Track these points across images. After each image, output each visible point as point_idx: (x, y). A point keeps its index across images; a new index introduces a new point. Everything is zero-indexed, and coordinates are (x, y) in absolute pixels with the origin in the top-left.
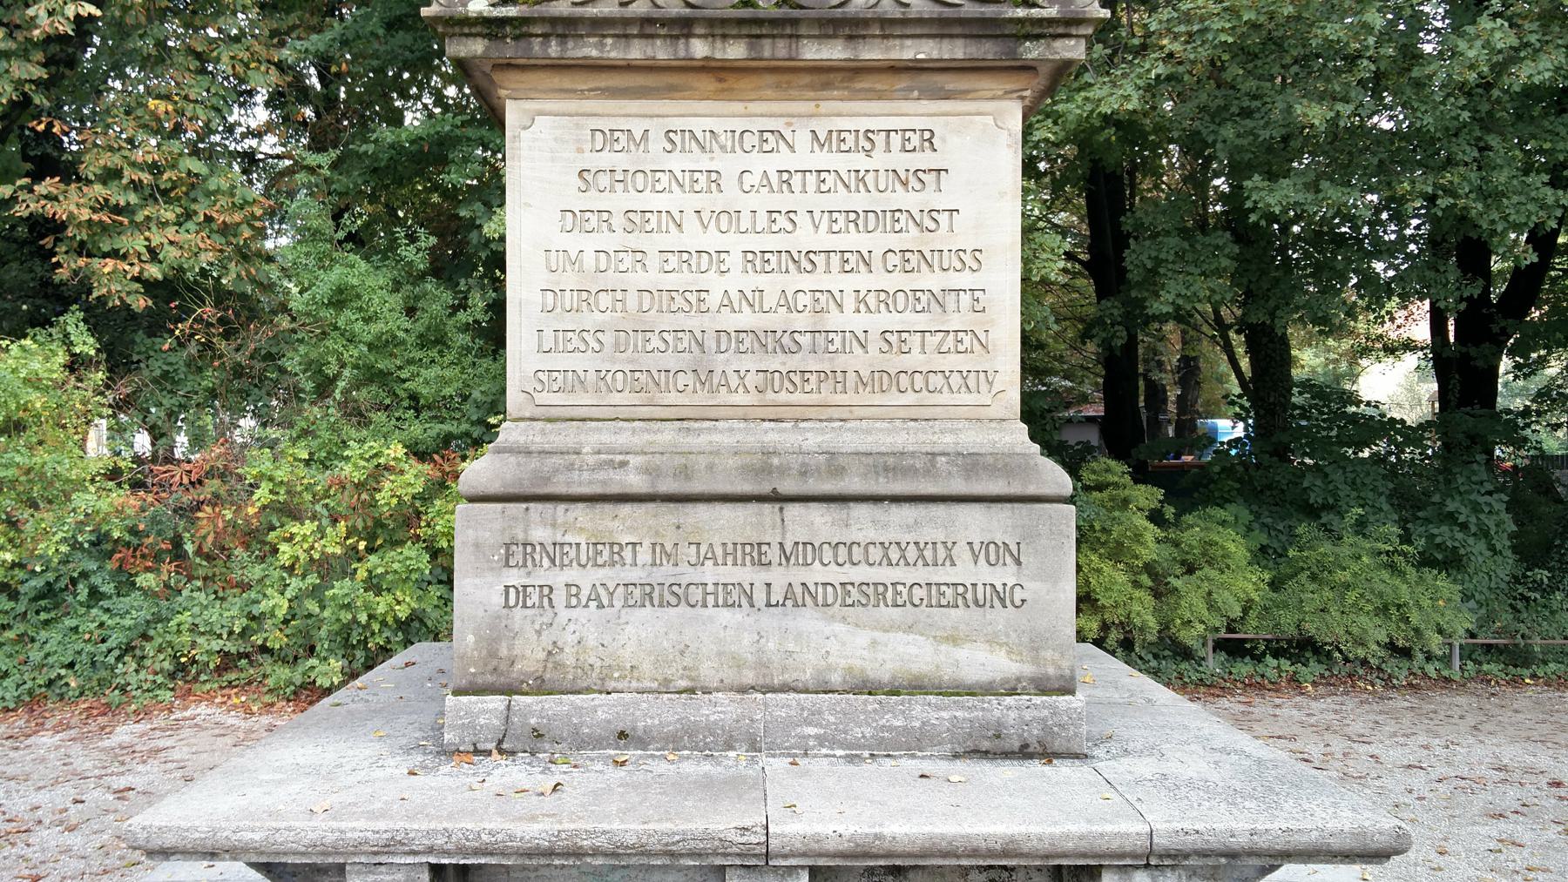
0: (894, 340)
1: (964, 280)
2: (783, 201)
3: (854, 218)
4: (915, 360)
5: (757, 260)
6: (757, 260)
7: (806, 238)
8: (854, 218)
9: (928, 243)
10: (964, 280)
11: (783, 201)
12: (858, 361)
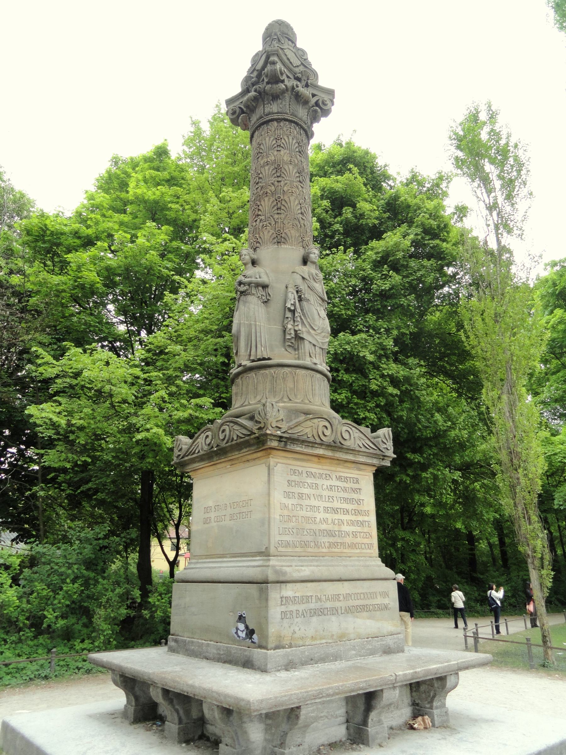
0: (355, 534)
2: (331, 494)
5: (326, 510)
6: (326, 510)
7: (336, 504)
9: (361, 508)
11: (331, 494)
12: (348, 540)
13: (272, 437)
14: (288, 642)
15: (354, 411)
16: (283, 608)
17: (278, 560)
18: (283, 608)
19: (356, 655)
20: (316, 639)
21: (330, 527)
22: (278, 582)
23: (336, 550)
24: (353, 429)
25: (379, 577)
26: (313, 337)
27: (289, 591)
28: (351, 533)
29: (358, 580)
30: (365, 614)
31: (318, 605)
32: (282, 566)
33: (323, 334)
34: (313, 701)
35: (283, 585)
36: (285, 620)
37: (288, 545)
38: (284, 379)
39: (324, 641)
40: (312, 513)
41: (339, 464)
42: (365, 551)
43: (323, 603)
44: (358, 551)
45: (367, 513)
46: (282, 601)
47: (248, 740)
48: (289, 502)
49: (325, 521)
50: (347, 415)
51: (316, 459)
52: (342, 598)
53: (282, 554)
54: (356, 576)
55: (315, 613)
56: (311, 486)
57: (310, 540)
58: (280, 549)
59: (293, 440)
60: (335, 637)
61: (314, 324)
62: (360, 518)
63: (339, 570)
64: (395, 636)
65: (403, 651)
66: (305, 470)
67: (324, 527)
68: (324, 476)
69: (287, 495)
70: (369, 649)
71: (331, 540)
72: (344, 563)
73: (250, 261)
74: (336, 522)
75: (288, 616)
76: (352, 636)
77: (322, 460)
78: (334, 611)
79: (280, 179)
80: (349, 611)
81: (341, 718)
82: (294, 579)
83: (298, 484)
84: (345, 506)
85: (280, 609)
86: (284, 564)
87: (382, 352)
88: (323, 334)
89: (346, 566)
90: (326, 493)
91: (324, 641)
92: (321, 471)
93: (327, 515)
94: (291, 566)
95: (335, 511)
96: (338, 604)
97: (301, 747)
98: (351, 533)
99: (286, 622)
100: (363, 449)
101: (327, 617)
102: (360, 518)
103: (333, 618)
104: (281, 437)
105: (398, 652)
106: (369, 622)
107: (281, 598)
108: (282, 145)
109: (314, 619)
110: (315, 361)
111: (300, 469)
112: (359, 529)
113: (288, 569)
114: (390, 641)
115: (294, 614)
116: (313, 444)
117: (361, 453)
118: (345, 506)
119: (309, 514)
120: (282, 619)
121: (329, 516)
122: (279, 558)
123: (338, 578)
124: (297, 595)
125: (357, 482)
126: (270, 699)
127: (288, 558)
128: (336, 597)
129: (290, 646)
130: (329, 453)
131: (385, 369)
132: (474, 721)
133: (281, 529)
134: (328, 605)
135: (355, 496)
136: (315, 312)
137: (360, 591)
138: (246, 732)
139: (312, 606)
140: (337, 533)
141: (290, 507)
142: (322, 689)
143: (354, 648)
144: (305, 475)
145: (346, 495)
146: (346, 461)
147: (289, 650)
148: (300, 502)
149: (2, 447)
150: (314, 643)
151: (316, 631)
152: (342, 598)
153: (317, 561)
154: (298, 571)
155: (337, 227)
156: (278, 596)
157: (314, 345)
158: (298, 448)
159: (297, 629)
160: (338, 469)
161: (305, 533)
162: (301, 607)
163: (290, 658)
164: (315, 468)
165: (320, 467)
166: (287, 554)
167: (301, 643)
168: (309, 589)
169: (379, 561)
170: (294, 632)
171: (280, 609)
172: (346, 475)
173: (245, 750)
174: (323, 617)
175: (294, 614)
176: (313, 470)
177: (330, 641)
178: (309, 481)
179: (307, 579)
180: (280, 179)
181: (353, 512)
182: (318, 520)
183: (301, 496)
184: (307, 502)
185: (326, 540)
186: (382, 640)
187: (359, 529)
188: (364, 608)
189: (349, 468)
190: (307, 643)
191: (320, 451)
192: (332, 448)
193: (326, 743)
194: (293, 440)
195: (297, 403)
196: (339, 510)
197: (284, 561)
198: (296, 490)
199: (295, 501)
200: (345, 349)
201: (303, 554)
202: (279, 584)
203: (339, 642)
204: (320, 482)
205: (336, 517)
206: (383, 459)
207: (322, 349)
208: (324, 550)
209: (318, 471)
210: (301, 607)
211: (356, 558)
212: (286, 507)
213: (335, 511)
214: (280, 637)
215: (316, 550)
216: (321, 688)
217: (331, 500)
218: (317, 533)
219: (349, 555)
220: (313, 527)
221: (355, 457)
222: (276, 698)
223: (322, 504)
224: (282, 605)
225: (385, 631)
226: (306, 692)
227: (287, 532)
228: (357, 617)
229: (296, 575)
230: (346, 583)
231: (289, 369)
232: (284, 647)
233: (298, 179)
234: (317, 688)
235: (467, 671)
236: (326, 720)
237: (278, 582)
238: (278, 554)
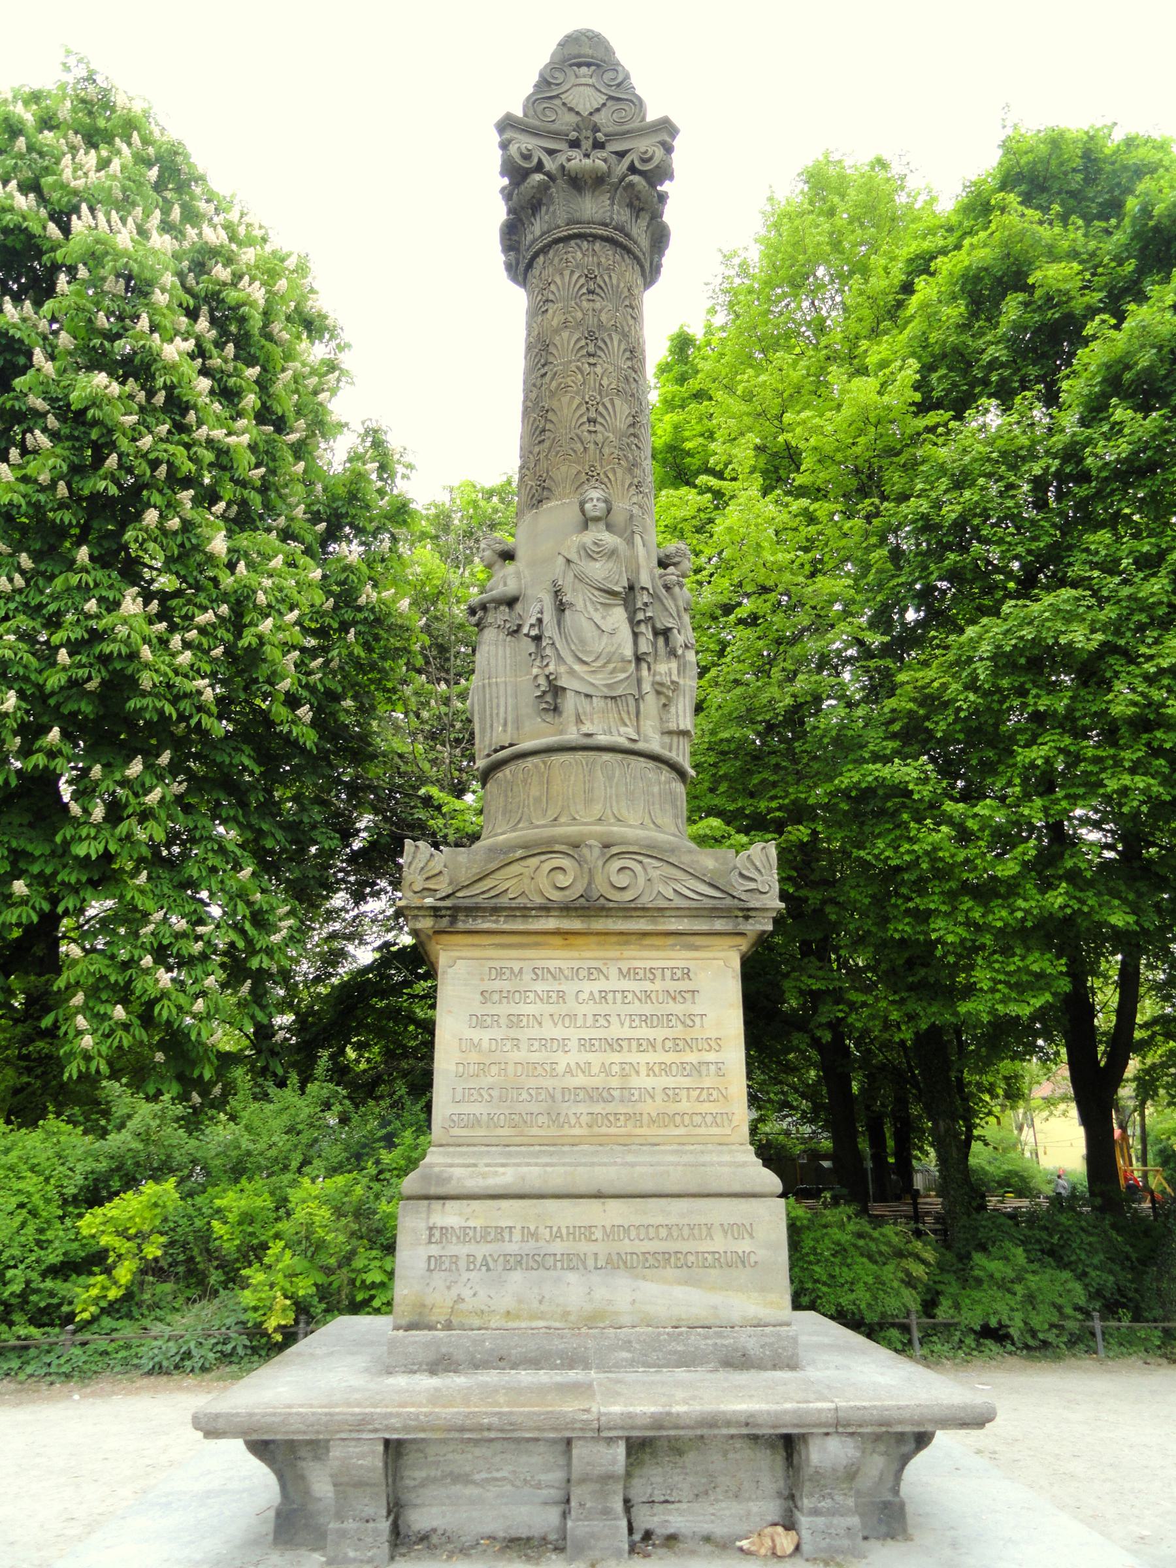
0: (671, 1094)
1: (711, 1057)
2: (603, 1009)
3: (645, 1019)
4: (684, 1106)
5: (586, 1045)
6: (586, 1045)
7: (616, 1031)
8: (645, 1019)
9: (696, 1033)
10: (711, 1057)
11: (603, 1009)
12: (649, 1108)
13: (416, 912)
14: (442, 1319)
15: (1093, 779)
16: (434, 1250)
17: (447, 1154)
18: (434, 1250)
19: (632, 1363)
20: (518, 1317)
21: (598, 1081)
22: (427, 1197)
23: (613, 1130)
24: (646, 860)
25: (725, 1189)
26: (582, 679)
27: (449, 1216)
28: (659, 1091)
29: (598, 1196)
30: (670, 1272)
31: (530, 1246)
32: (451, 1166)
33: (611, 666)
34: (354, 1435)
35: (436, 1205)
36: (436, 1275)
37: (476, 1122)
38: (525, 781)
39: (541, 1324)
40: (544, 1054)
41: (627, 943)
42: (702, 1130)
43: (541, 1243)
44: (681, 1131)
45: (716, 1044)
46: (431, 1236)
47: (307, 1492)
48: (484, 1036)
49: (586, 1068)
50: (1081, 791)
51: (558, 941)
52: (598, 1234)
53: (461, 1141)
54: (649, 1186)
55: (520, 1262)
56: (546, 998)
57: (535, 1110)
58: (456, 1131)
59: (473, 911)
60: (572, 1318)
61: (585, 652)
62: (692, 1057)
63: (607, 1174)
64: (768, 1330)
65: (792, 1365)
66: (527, 966)
67: (580, 1080)
68: (583, 973)
69: (479, 1021)
70: (675, 1352)
71: (598, 1108)
72: (630, 1158)
73: (496, 557)
74: (616, 1068)
75: (446, 1265)
76: (626, 1320)
77: (572, 940)
78: (574, 1262)
79: (592, 360)
80: (617, 1263)
81: (552, 1491)
82: (464, 1191)
83: (507, 996)
84: (644, 1032)
85: (423, 1252)
86: (457, 1161)
87: (1143, 618)
88: (611, 666)
89: (633, 1165)
90: (589, 1009)
91: (541, 1324)
92: (576, 964)
93: (590, 1057)
94: (475, 1165)
95: (615, 1045)
96: (584, 1247)
97: (371, 1525)
98: (659, 1091)
99: (439, 1279)
100: (679, 902)
101: (552, 1273)
102: (692, 1057)
103: (572, 1277)
104: (435, 909)
105: (776, 1365)
106: (679, 1292)
107: (431, 1229)
108: (598, 290)
109: (517, 1276)
110: (587, 728)
111: (516, 966)
112: (685, 1082)
113: (458, 1172)
114: (749, 1341)
115: (462, 1264)
116: (525, 912)
117: (668, 913)
118: (644, 1032)
119: (536, 1057)
120: (429, 1270)
121: (595, 1059)
122: (451, 1149)
123: (592, 1189)
124: (471, 1224)
125: (687, 974)
126: (237, 1415)
127: (464, 1149)
128: (585, 1232)
129: (448, 1326)
130: (576, 924)
131: (1150, 658)
132: (416, 1505)
133: (459, 1090)
134: (558, 1247)
135: (677, 1008)
136: (586, 624)
137: (660, 1220)
138: (302, 1477)
139: (512, 1248)
140: (616, 1093)
141: (485, 1044)
142: (372, 1414)
143: (627, 1345)
144: (527, 976)
145: (647, 1009)
146: (645, 934)
147: (441, 1334)
148: (513, 1033)
149: (1171, 931)
150: (510, 1325)
151: (520, 1301)
152: (598, 1234)
153: (551, 1154)
154: (484, 1176)
155: (992, 352)
156: (422, 1225)
157: (588, 696)
158: (471, 924)
159: (467, 1293)
160: (627, 954)
161: (525, 1096)
162: (482, 1251)
163: (444, 1350)
164: (557, 958)
165: (575, 954)
166: (476, 1141)
167: (477, 1322)
168: (508, 1213)
169: (748, 1155)
170: (460, 1299)
171: (423, 1252)
172: (649, 964)
173: (295, 1510)
174: (541, 1272)
175: (462, 1264)
176: (552, 965)
177: (557, 1325)
178: (540, 987)
179: (501, 1192)
180: (592, 360)
181: (669, 1044)
182: (561, 1068)
183: (515, 1021)
184: (535, 1032)
185: (582, 1109)
186: (720, 1335)
187: (685, 1082)
188: (665, 1259)
189: (657, 948)
190: (493, 1325)
191: (551, 924)
192: (580, 913)
193: (501, 1534)
194: (473, 911)
195: (538, 827)
196: (624, 1044)
197: (462, 1154)
198: (503, 1009)
199: (497, 1033)
200: (1021, 638)
201: (518, 1140)
202: (426, 1202)
203: (583, 1330)
204: (571, 988)
205: (616, 1057)
206: (747, 918)
207: (613, 698)
208: (577, 1131)
209: (563, 965)
210: (482, 1251)
211: (675, 1147)
212: (476, 1046)
213: (615, 1045)
214: (424, 1306)
215: (553, 1131)
216: (367, 1410)
217: (602, 1021)
218: (558, 1096)
219: (655, 1140)
220: (548, 1083)
221: (656, 923)
222: (251, 1415)
223: (574, 1034)
224: (430, 1242)
225: (735, 1316)
226: (326, 1414)
227: (476, 1096)
228: (644, 1278)
229: (473, 1184)
230: (612, 1204)
231: (535, 760)
232: (431, 1328)
233: (584, 352)
234: (357, 1410)
235: (963, 1432)
236: (509, 1487)
237: (427, 1197)
238: (451, 1141)
